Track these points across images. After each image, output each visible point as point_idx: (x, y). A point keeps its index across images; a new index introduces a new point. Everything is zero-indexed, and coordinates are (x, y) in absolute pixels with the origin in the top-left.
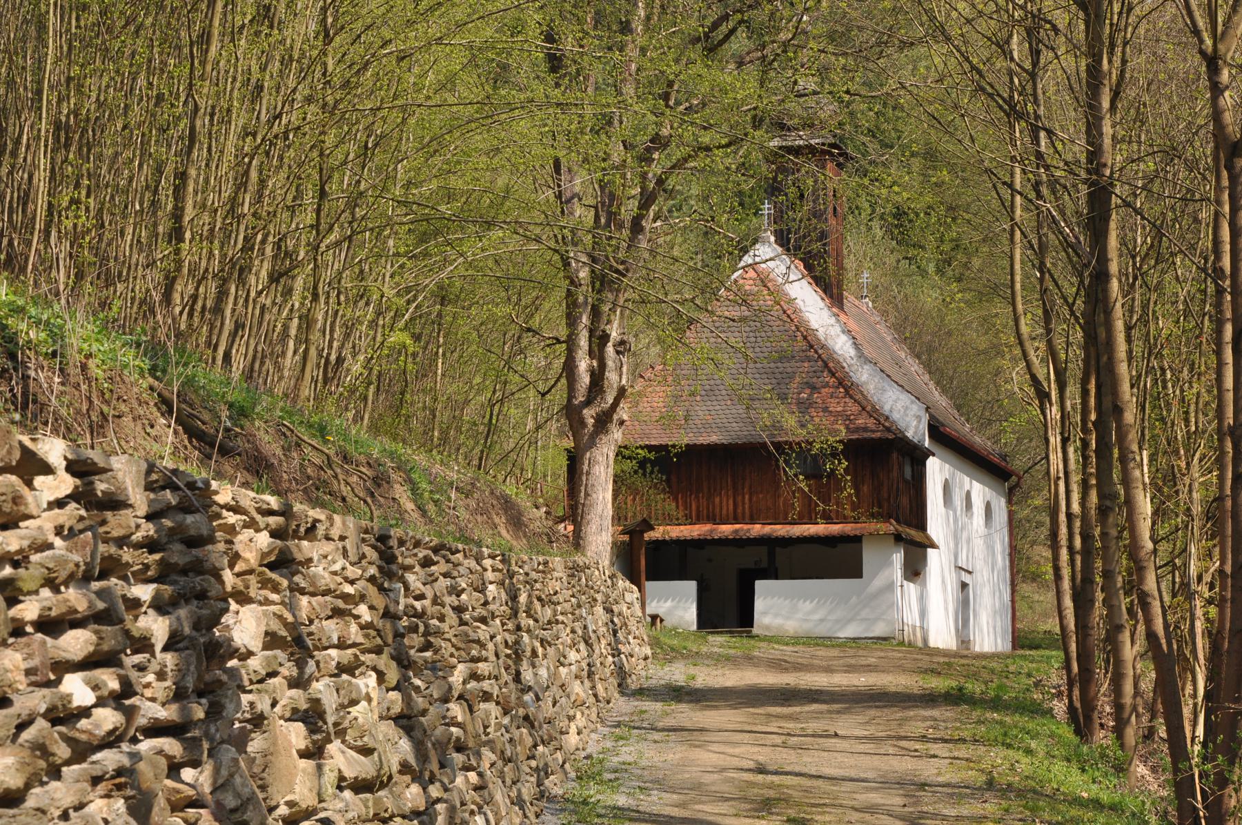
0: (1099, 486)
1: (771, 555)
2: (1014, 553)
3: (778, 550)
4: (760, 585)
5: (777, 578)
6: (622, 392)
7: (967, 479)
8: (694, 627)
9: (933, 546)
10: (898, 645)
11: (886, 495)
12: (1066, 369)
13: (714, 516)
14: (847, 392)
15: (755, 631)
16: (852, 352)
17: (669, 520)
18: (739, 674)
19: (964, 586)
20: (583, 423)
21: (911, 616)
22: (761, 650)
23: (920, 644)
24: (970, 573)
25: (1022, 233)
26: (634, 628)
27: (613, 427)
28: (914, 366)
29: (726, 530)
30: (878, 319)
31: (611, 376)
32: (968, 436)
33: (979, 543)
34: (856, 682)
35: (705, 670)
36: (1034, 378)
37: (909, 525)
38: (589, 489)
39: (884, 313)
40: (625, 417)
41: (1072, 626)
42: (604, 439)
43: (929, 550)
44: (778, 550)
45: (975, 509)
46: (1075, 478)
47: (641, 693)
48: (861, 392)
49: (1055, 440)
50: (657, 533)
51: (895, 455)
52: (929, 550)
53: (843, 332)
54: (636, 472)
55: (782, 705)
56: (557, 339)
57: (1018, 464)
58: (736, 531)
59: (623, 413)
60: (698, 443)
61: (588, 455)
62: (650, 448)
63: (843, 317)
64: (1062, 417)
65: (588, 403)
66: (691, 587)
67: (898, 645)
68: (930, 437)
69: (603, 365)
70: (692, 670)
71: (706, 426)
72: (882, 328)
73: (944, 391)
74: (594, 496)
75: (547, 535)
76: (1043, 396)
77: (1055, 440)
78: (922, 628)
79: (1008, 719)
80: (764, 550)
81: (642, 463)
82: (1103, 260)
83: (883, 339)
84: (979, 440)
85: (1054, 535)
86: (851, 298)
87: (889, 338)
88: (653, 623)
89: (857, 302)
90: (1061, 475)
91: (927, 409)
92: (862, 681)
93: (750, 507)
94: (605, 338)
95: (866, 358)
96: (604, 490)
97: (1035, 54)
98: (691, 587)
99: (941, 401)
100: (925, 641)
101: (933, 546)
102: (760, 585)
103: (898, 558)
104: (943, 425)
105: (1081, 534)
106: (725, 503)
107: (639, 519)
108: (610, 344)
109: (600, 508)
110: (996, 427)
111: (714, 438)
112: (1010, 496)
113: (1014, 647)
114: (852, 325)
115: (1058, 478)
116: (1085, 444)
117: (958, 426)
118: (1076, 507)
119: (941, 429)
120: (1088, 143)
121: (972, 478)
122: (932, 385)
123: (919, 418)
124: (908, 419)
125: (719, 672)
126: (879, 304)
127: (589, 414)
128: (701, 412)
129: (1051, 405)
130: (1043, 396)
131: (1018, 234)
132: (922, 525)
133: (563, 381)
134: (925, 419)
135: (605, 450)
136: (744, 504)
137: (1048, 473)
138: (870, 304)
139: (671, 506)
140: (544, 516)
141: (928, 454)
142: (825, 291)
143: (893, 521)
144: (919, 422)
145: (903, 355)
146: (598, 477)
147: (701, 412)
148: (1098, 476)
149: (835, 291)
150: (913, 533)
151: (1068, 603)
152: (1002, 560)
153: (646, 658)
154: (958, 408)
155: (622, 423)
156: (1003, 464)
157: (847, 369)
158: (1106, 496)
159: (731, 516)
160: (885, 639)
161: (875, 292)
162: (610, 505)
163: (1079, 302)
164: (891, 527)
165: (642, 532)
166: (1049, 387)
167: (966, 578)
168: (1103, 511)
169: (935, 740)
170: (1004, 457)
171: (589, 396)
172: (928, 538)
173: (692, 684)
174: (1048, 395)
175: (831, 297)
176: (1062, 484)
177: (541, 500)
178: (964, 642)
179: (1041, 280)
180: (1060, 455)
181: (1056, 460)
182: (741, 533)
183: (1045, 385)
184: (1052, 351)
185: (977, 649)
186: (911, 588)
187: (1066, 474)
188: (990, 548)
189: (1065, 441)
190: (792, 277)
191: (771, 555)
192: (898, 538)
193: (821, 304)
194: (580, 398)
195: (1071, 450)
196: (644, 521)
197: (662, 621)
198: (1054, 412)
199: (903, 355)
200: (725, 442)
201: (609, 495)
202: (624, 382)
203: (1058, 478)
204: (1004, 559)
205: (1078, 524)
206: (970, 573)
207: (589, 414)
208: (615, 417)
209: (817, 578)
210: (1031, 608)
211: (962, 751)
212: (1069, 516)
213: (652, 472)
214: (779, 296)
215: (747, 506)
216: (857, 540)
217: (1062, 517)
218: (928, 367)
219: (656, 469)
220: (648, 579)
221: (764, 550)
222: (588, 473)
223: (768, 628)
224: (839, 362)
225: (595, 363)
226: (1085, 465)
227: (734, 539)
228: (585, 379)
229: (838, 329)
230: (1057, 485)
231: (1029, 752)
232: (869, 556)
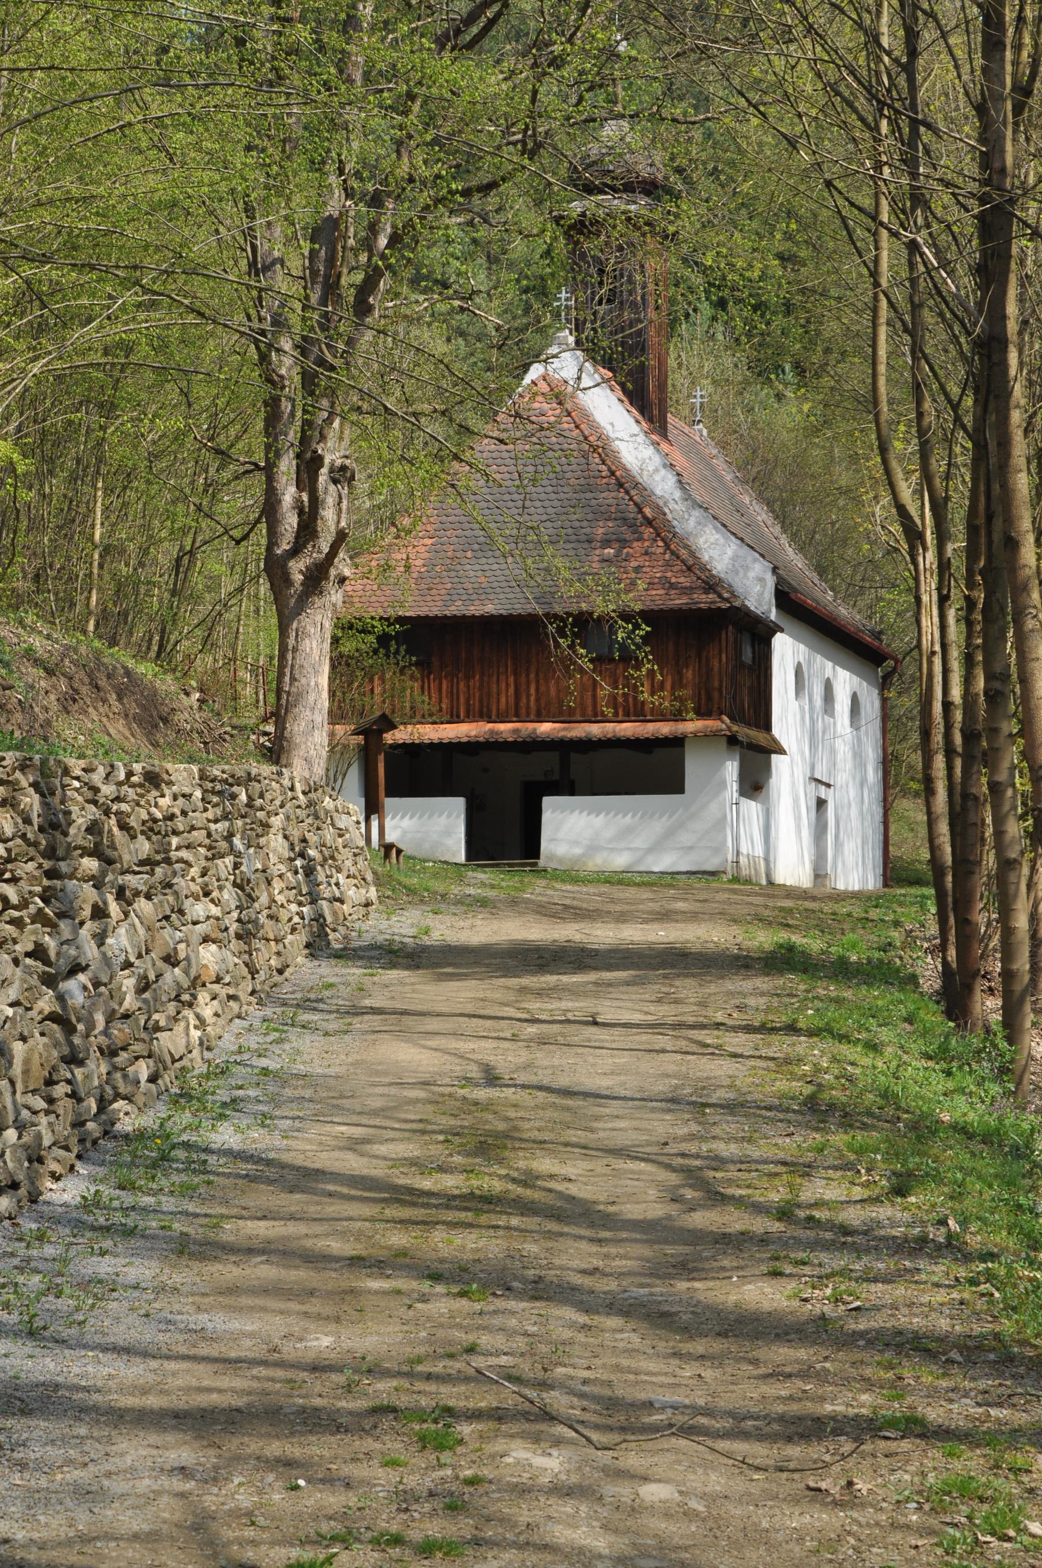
0: (987, 664)
1: (565, 764)
2: (888, 762)
3: (574, 756)
4: (547, 801)
5: (572, 793)
6: (341, 536)
7: (829, 665)
8: (461, 857)
9: (781, 751)
10: (730, 881)
11: (716, 684)
12: (947, 498)
13: (489, 711)
14: (667, 546)
15: (542, 862)
16: (678, 494)
17: (415, 716)
18: (495, 925)
19: (821, 803)
20: (288, 581)
21: (752, 846)
22: (537, 889)
23: (764, 882)
24: (828, 786)
25: (890, 303)
26: (348, 863)
27: (330, 586)
28: (761, 515)
29: (505, 729)
30: (715, 452)
31: (328, 514)
32: (831, 608)
33: (843, 749)
34: (652, 937)
35: (448, 920)
36: (902, 510)
37: (748, 724)
38: (296, 672)
39: (723, 445)
40: (347, 572)
41: (948, 859)
42: (318, 602)
43: (774, 757)
44: (574, 756)
45: (838, 707)
46: (954, 653)
47: (346, 954)
48: (687, 547)
49: (929, 597)
50: (400, 735)
51: (730, 628)
52: (774, 757)
53: (665, 466)
54: (375, 652)
55: (534, 973)
56: (256, 465)
57: (896, 645)
58: (516, 731)
59: (343, 566)
60: (468, 613)
61: (295, 625)
62: (401, 620)
63: (664, 446)
64: (940, 566)
65: (295, 551)
66: (458, 804)
67: (730, 881)
68: (779, 606)
69: (315, 502)
70: (430, 921)
71: (481, 592)
72: (719, 463)
73: (801, 549)
74: (303, 681)
75: (200, 733)
76: (914, 535)
77: (929, 597)
78: (767, 860)
79: (848, 994)
80: (554, 756)
81: (383, 640)
82: (998, 316)
83: (720, 479)
84: (845, 613)
85: (926, 734)
86: (681, 424)
87: (729, 477)
88: (387, 856)
89: (687, 429)
90: (937, 648)
91: (775, 570)
92: (661, 934)
93: (538, 700)
94: (317, 461)
95: (694, 502)
96: (316, 672)
97: (911, 37)
98: (458, 804)
99: (795, 560)
100: (768, 875)
101: (781, 751)
102: (547, 801)
103: (731, 769)
104: (796, 591)
105: (962, 730)
106: (504, 699)
107: (378, 714)
108: (324, 471)
109: (311, 698)
110: (870, 596)
111: (490, 608)
112: (884, 684)
113: (886, 885)
114: (679, 458)
115: (933, 653)
116: (970, 603)
117: (818, 594)
118: (956, 693)
119: (793, 596)
120: (982, 140)
121: (837, 662)
122: (784, 540)
123: (761, 580)
124: (748, 583)
125: (468, 923)
126: (718, 434)
127: (297, 569)
128: (473, 572)
129: (925, 549)
130: (914, 535)
131: (884, 303)
132: (766, 725)
133: (263, 527)
134: (770, 581)
135: (319, 618)
136: (528, 696)
137: (919, 646)
138: (705, 432)
139: (424, 702)
140: (196, 705)
141: (772, 630)
142: (642, 412)
143: (725, 718)
144: (764, 586)
145: (747, 500)
146: (309, 655)
147: (473, 572)
148: (985, 648)
149: (656, 412)
150: (757, 736)
151: (943, 828)
152: (873, 775)
153: (368, 904)
154: (821, 571)
155: (342, 580)
156: (876, 643)
157: (669, 516)
158: (997, 677)
159: (533, 711)
160: (713, 874)
161: (711, 414)
162: (325, 695)
163: (969, 402)
164: (722, 724)
165: (381, 732)
166: (922, 516)
167: (823, 792)
168: (994, 697)
169: (735, 1029)
170: (878, 635)
171: (296, 542)
172: (775, 740)
173: (426, 941)
174: (921, 536)
175: (651, 420)
176: (937, 661)
177: (194, 683)
178: (819, 875)
179: (915, 368)
180: (936, 620)
181: (930, 623)
182: (497, 733)
183: (918, 521)
184: (927, 476)
185: (841, 886)
186: (751, 808)
187: (944, 646)
188: (857, 755)
189: (943, 600)
190: (586, 382)
191: (565, 764)
192: (732, 741)
193: (635, 429)
194: (285, 545)
195: (951, 615)
196: (384, 716)
197: (399, 852)
198: (929, 559)
199: (747, 500)
200: (504, 612)
201: (324, 680)
202: (343, 524)
203: (933, 653)
204: (876, 770)
205: (958, 716)
206: (828, 786)
207: (297, 569)
208: (333, 572)
209: (626, 794)
210: (912, 830)
211: (780, 1046)
212: (947, 705)
213: (397, 652)
214: (580, 418)
215: (532, 698)
216: (677, 742)
217: (937, 708)
218: (783, 519)
219: (403, 648)
220: (390, 794)
221: (554, 756)
222: (295, 650)
223: (551, 857)
224: (658, 507)
225: (305, 497)
226: (969, 636)
227: (515, 742)
228: (290, 521)
229: (657, 460)
230: (930, 663)
231: (873, 1047)
232: (694, 766)
